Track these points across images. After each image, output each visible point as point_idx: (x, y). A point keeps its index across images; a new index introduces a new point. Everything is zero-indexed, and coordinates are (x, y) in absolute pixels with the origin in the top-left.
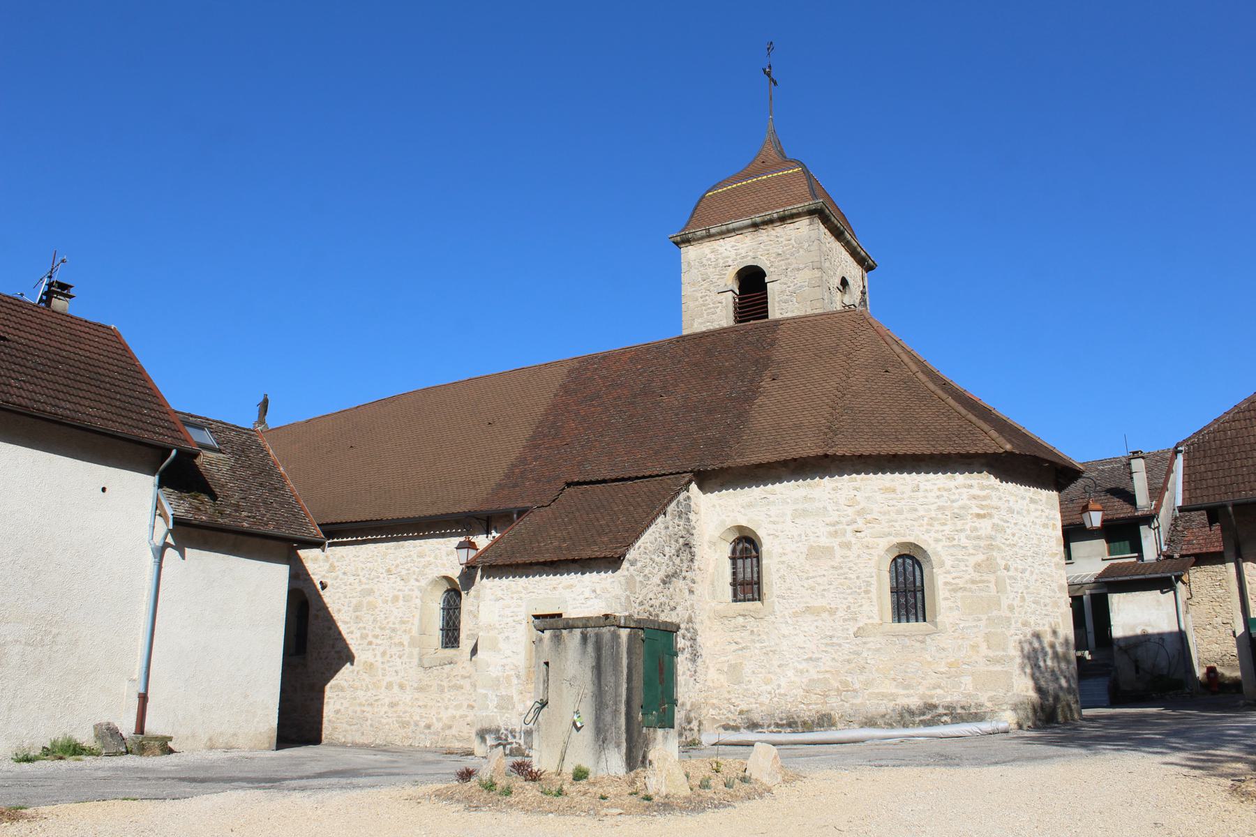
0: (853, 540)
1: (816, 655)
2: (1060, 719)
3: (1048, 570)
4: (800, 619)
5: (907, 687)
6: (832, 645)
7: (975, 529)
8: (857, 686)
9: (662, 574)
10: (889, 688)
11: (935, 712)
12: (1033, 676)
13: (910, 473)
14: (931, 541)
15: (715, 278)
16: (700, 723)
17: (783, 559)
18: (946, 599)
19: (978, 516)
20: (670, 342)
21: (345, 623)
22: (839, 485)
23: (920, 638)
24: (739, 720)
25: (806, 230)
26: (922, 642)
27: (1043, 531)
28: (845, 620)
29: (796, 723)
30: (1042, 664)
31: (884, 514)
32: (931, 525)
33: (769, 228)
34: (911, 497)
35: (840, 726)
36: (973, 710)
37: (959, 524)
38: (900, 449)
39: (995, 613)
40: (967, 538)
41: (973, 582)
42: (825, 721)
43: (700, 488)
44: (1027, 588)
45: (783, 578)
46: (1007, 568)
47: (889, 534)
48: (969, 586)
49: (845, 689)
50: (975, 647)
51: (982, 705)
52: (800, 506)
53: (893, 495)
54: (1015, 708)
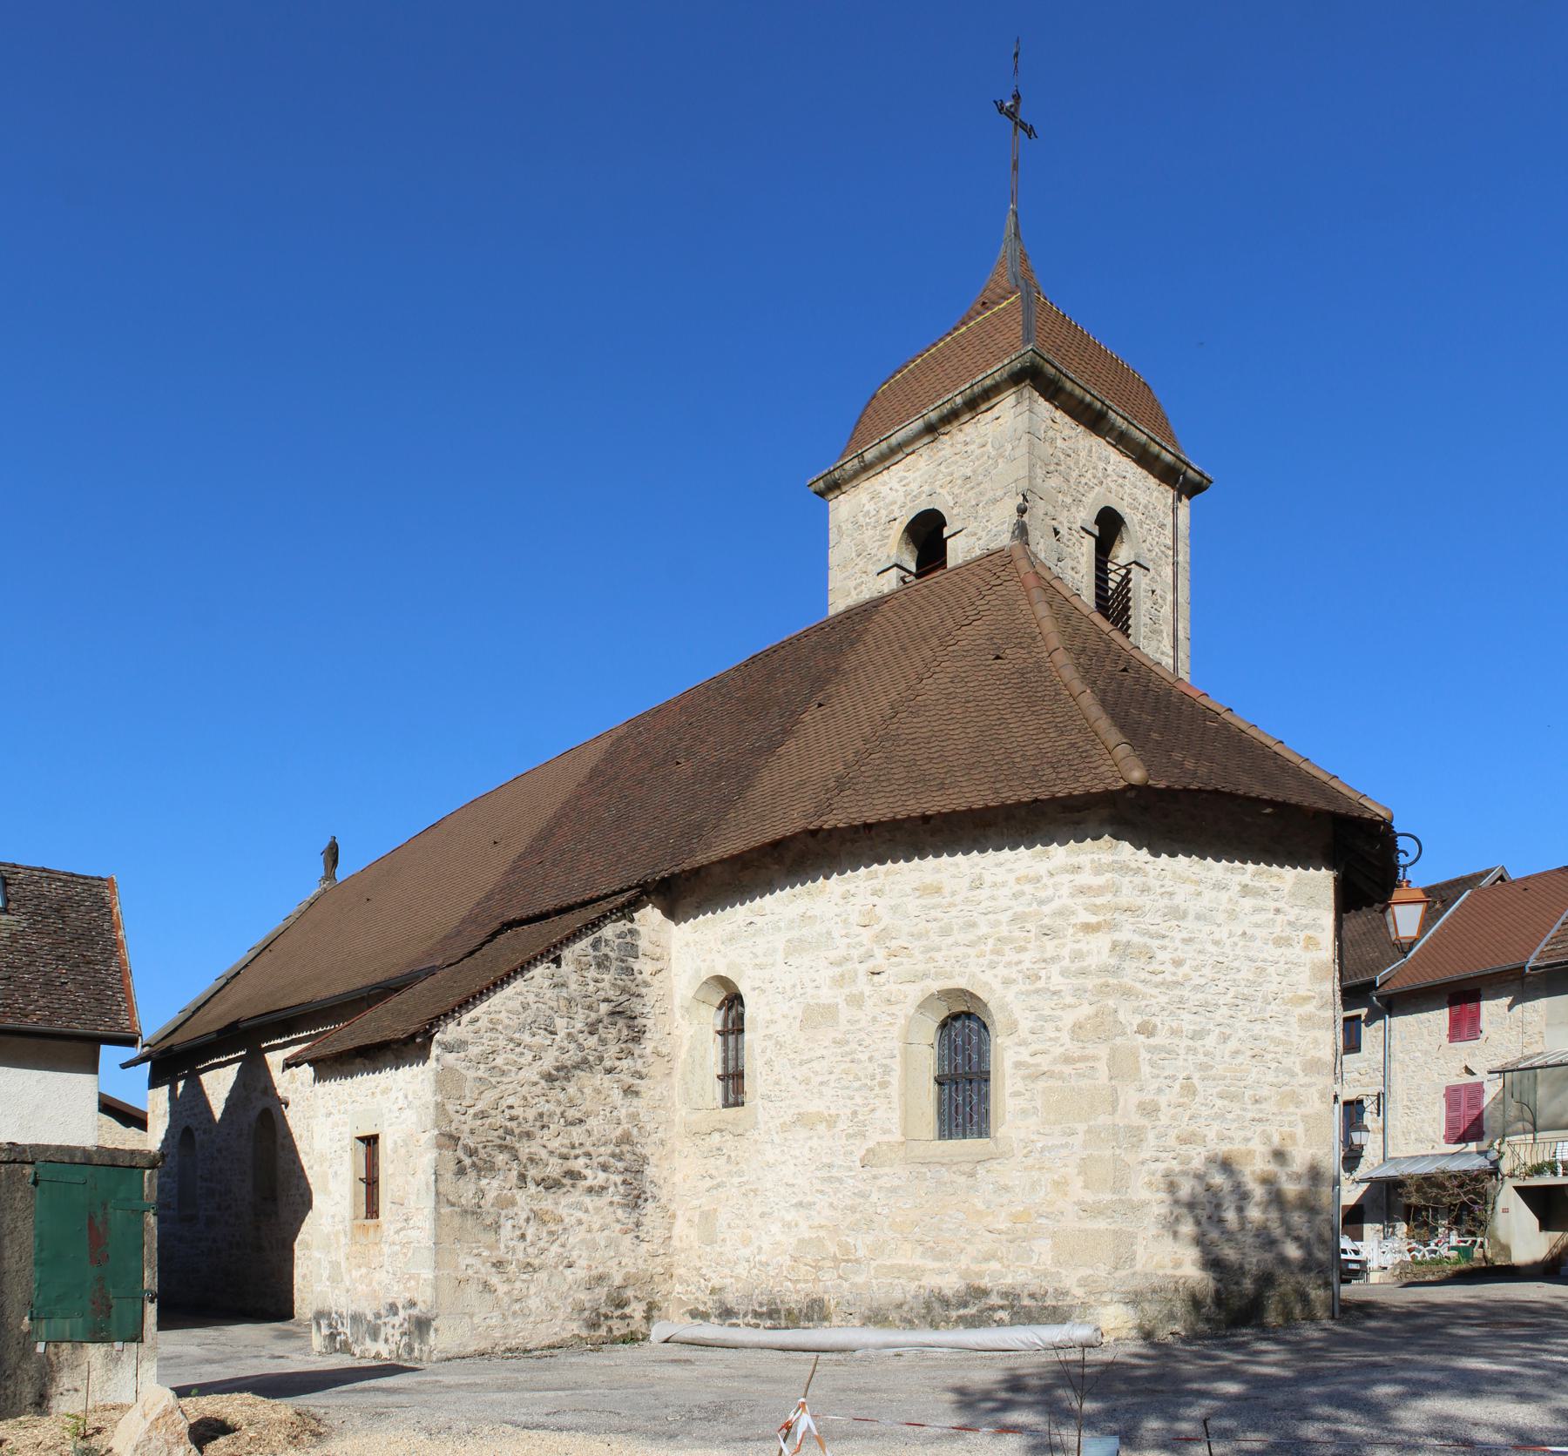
1: (809, 1199)
2: (1272, 1318)
3: (1277, 1031)
4: (789, 1135)
5: (942, 1256)
6: (830, 1179)
7: (1078, 956)
8: (861, 1253)
10: (907, 1256)
11: (982, 1304)
12: (1199, 1241)
13: (967, 852)
14: (996, 985)
15: (872, 547)
17: (770, 1031)
18: (1017, 1094)
19: (1088, 928)
21: (306, 1154)
22: (851, 887)
23: (967, 1168)
24: (710, 1304)
25: (1014, 417)
26: (972, 1175)
27: (1273, 952)
28: (849, 1136)
29: (778, 1311)
31: (919, 936)
34: (966, 901)
35: (835, 1320)
36: (1050, 1302)
37: (1050, 946)
38: (935, 804)
39: (1103, 1119)
40: (1062, 973)
41: (1067, 1060)
42: (815, 1312)
43: (945, 524)
44: (1203, 1067)
45: (769, 1063)
46: (1146, 1030)
47: (925, 975)
48: (1057, 1068)
49: (846, 1259)
50: (1061, 1185)
51: (1067, 1293)
52: (795, 934)
53: (936, 900)
54: (1134, 1299)
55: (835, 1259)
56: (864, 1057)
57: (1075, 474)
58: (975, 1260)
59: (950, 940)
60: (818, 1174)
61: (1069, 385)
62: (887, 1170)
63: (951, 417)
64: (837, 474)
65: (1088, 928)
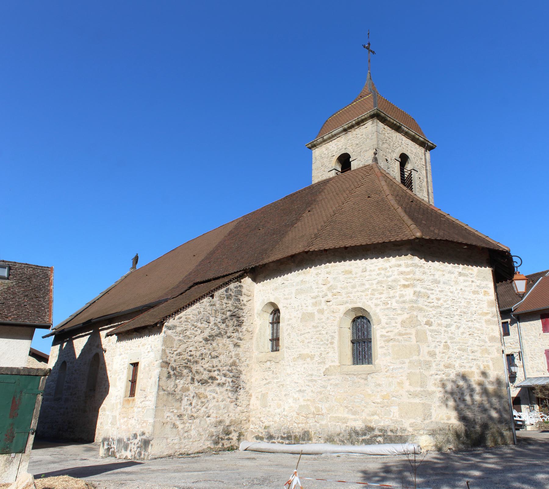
0: (325, 307)
1: (304, 388)
2: (490, 443)
3: (477, 325)
6: (312, 381)
7: (402, 296)
8: (324, 411)
9: (206, 334)
10: (342, 413)
11: (372, 434)
12: (457, 408)
13: (360, 259)
14: (372, 306)
15: (327, 164)
16: (240, 435)
17: (290, 322)
18: (382, 347)
19: (405, 286)
20: (281, 200)
23: (364, 376)
24: (264, 433)
25: (371, 127)
28: (319, 363)
29: (291, 436)
30: (468, 398)
31: (344, 288)
32: (373, 294)
33: (352, 130)
34: (361, 276)
36: (399, 434)
37: (392, 292)
38: (349, 243)
39: (415, 358)
40: (397, 302)
41: (400, 334)
42: (306, 437)
45: (289, 334)
46: (429, 323)
47: (347, 302)
48: (397, 337)
49: (318, 414)
50: (400, 384)
51: (405, 430)
52: (299, 287)
53: (350, 276)
54: (433, 433)
55: (314, 414)
56: (324, 332)
57: (392, 144)
58: (368, 415)
59: (355, 290)
60: (307, 378)
61: (389, 119)
62: (333, 377)
63: (352, 127)
64: (315, 143)
65: (405, 286)
